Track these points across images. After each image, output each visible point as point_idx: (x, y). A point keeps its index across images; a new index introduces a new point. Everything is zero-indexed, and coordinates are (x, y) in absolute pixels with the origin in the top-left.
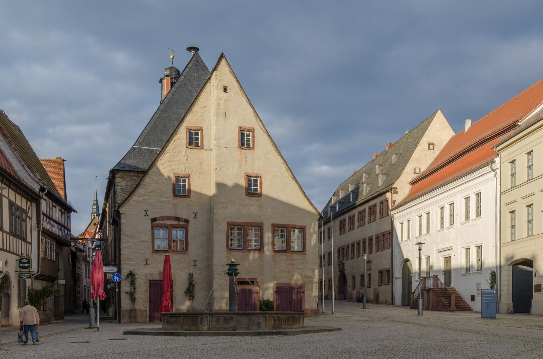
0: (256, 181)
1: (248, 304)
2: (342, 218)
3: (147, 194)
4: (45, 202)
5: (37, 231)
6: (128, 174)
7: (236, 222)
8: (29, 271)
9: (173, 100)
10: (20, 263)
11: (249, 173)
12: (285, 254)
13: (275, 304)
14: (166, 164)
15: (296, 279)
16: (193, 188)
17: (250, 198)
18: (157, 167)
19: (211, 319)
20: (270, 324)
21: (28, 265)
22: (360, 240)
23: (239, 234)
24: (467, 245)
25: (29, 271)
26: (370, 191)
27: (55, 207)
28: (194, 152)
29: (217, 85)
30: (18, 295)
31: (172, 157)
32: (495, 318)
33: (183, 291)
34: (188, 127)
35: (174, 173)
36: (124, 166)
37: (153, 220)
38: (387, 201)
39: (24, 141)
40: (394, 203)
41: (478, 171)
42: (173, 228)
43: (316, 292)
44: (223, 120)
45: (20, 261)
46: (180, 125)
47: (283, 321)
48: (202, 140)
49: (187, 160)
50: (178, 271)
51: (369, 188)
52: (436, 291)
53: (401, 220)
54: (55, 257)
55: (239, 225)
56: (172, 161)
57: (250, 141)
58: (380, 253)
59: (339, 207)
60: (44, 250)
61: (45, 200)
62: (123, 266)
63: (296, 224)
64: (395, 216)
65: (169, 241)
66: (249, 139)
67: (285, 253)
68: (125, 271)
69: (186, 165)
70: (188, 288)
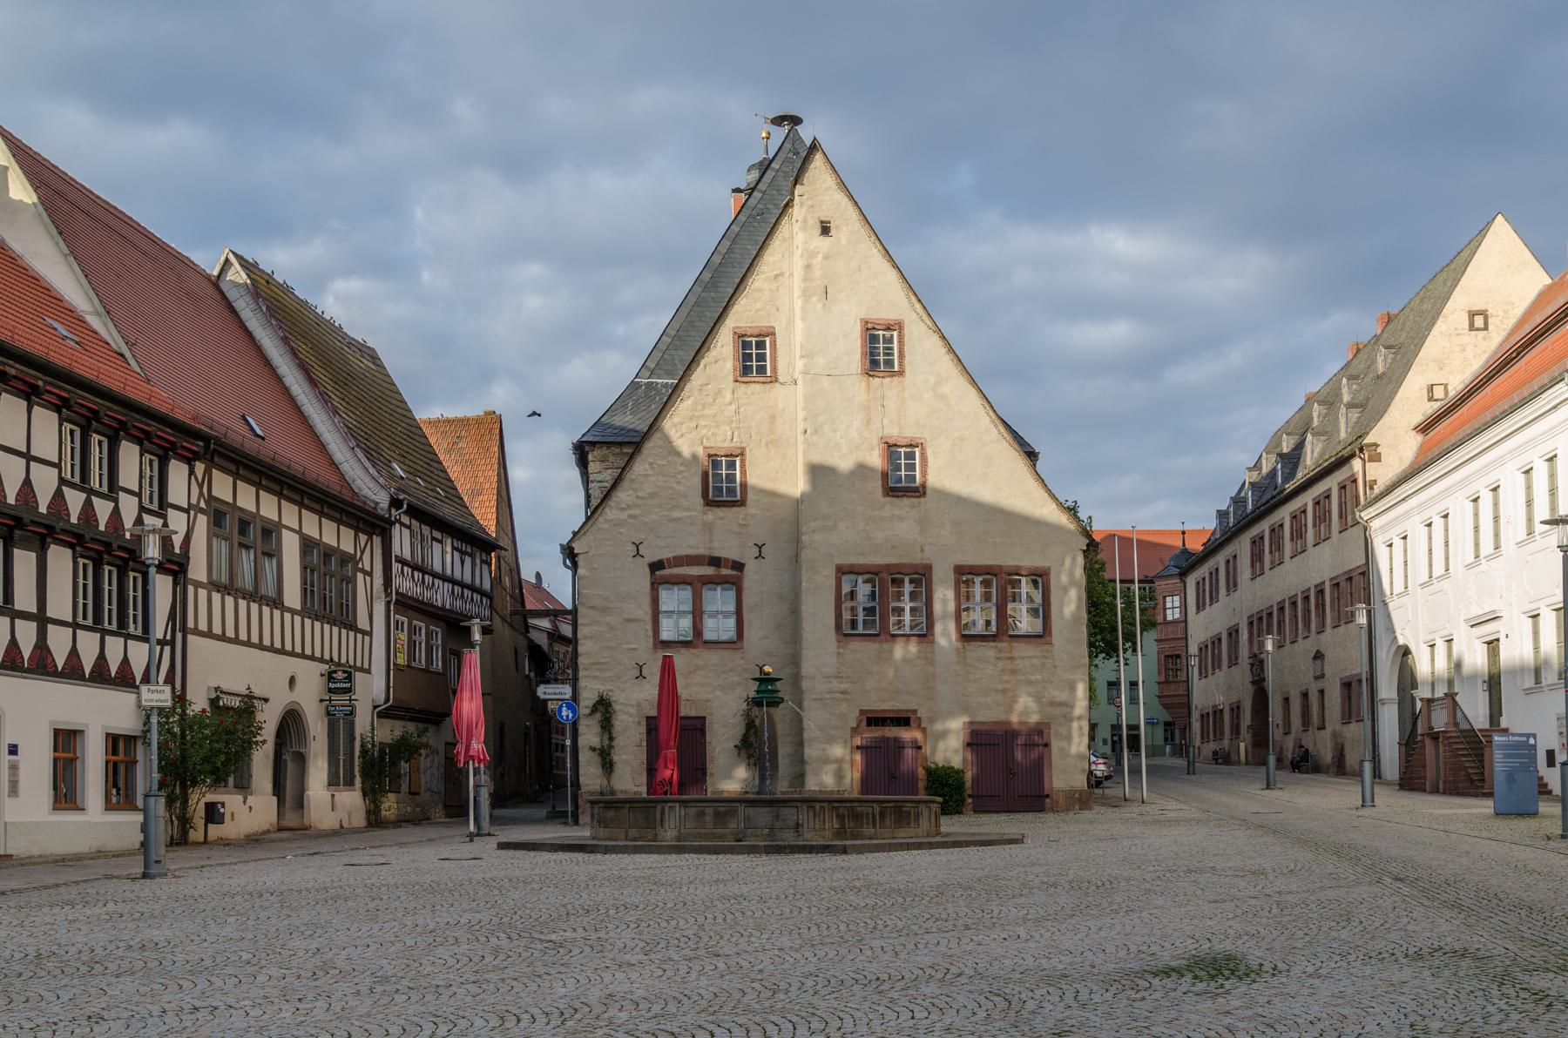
0: (910, 456)
1: (1014, 774)
2: (1254, 531)
3: (640, 502)
4: (406, 532)
5: (383, 603)
6: (618, 450)
7: (861, 565)
8: (350, 700)
9: (732, 255)
10: (329, 681)
11: (891, 437)
12: (992, 644)
13: (969, 775)
14: (685, 425)
15: (1025, 710)
16: (752, 480)
17: (895, 500)
18: (664, 433)
19: (683, 813)
20: (827, 826)
21: (348, 685)
22: (1297, 595)
23: (913, 596)
24: (1534, 606)
25: (350, 700)
26: (1322, 454)
27: (440, 542)
28: (754, 391)
29: (805, 221)
30: (329, 756)
31: (700, 407)
32: (1534, 814)
33: (732, 745)
34: (737, 331)
35: (705, 448)
36: (610, 430)
37: (656, 566)
38: (1355, 481)
39: (384, 384)
40: (1372, 488)
41: (1543, 396)
42: (704, 584)
43: (1079, 744)
44: (819, 306)
45: (330, 677)
46: (718, 326)
47: (868, 819)
48: (774, 359)
49: (737, 412)
50: (718, 693)
51: (1320, 445)
52: (1450, 737)
53: (1386, 537)
54: (440, 664)
55: (868, 573)
56: (698, 417)
57: (892, 355)
58: (1342, 629)
59: (1253, 500)
60: (406, 647)
61: (409, 527)
62: (582, 683)
63: (1021, 564)
64: (1375, 524)
65: (694, 618)
66: (892, 349)
67: (994, 641)
68: (588, 697)
69: (734, 425)
70: (744, 735)
